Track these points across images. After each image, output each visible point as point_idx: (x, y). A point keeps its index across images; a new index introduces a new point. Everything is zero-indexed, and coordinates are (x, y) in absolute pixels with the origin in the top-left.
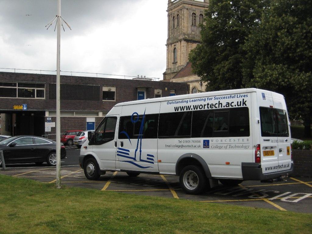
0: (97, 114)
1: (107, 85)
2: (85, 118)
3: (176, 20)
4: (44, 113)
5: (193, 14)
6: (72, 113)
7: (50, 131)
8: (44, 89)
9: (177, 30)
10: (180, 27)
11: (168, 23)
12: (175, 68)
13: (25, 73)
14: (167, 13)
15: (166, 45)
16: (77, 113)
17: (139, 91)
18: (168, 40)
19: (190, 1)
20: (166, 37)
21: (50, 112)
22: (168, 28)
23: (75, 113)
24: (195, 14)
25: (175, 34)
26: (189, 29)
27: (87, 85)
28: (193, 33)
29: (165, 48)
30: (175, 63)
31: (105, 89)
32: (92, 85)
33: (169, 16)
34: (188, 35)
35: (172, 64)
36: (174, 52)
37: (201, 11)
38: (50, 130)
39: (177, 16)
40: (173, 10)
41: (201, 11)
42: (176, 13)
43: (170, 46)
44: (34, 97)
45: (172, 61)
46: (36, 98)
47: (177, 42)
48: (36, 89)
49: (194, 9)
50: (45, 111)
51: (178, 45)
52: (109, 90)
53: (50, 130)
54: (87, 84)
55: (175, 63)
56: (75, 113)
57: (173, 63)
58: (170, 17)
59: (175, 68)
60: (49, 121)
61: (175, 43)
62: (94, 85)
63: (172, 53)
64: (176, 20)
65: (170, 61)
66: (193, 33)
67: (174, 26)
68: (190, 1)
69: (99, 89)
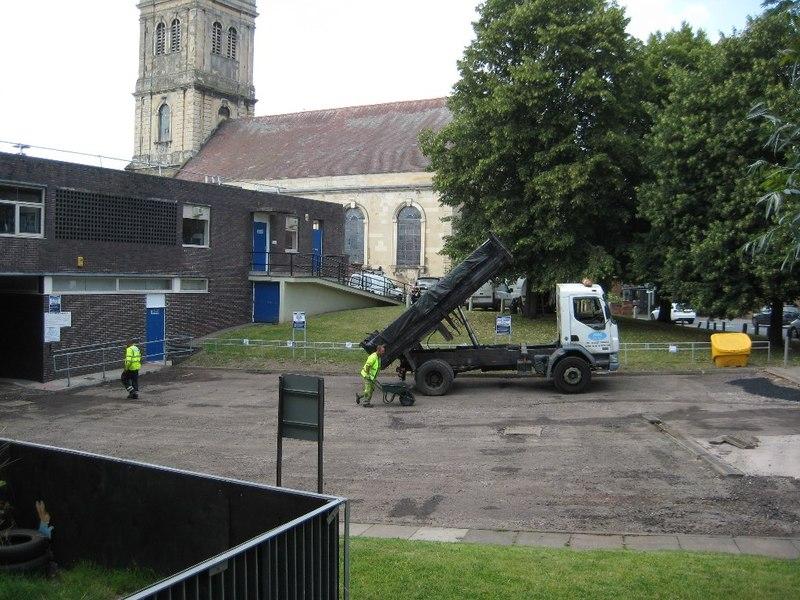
0: (168, 284)
1: (194, 203)
2: (142, 298)
3: (168, 36)
4: (41, 280)
5: (215, 24)
6: (111, 282)
7: (58, 339)
8: (41, 206)
9: (173, 59)
10: (184, 54)
11: (141, 38)
12: (165, 156)
13: (55, 159)
14: (139, 12)
15: (134, 95)
16: (124, 282)
17: (256, 220)
18: (142, 81)
19: (240, 4)
20: (134, 74)
21: (56, 280)
22: (140, 50)
23: (118, 281)
24: (219, 26)
25: (163, 67)
26: (207, 61)
27: (149, 199)
28: (215, 72)
29: (132, 102)
30: (162, 143)
31: (189, 212)
32: (159, 200)
33: (144, 19)
34: (203, 75)
35: (153, 147)
36: (160, 115)
37: (232, 21)
38: (57, 338)
39: (174, 23)
40: (158, 8)
41: (232, 21)
42: (168, 18)
43: (147, 98)
44: (12, 230)
45: (155, 137)
46: (18, 234)
47: (173, 91)
48: (18, 204)
49: (218, 13)
50: (43, 277)
51: (175, 99)
52: (198, 216)
53: (57, 338)
54: (150, 196)
55: (162, 143)
56: (118, 281)
57: (159, 143)
58: (149, 24)
59: (162, 157)
60: (56, 309)
61: (165, 92)
62: (166, 200)
63: (155, 118)
64: (168, 36)
65: (146, 137)
66: (215, 72)
67: (160, 47)
68: (240, 4)
69: (174, 210)
